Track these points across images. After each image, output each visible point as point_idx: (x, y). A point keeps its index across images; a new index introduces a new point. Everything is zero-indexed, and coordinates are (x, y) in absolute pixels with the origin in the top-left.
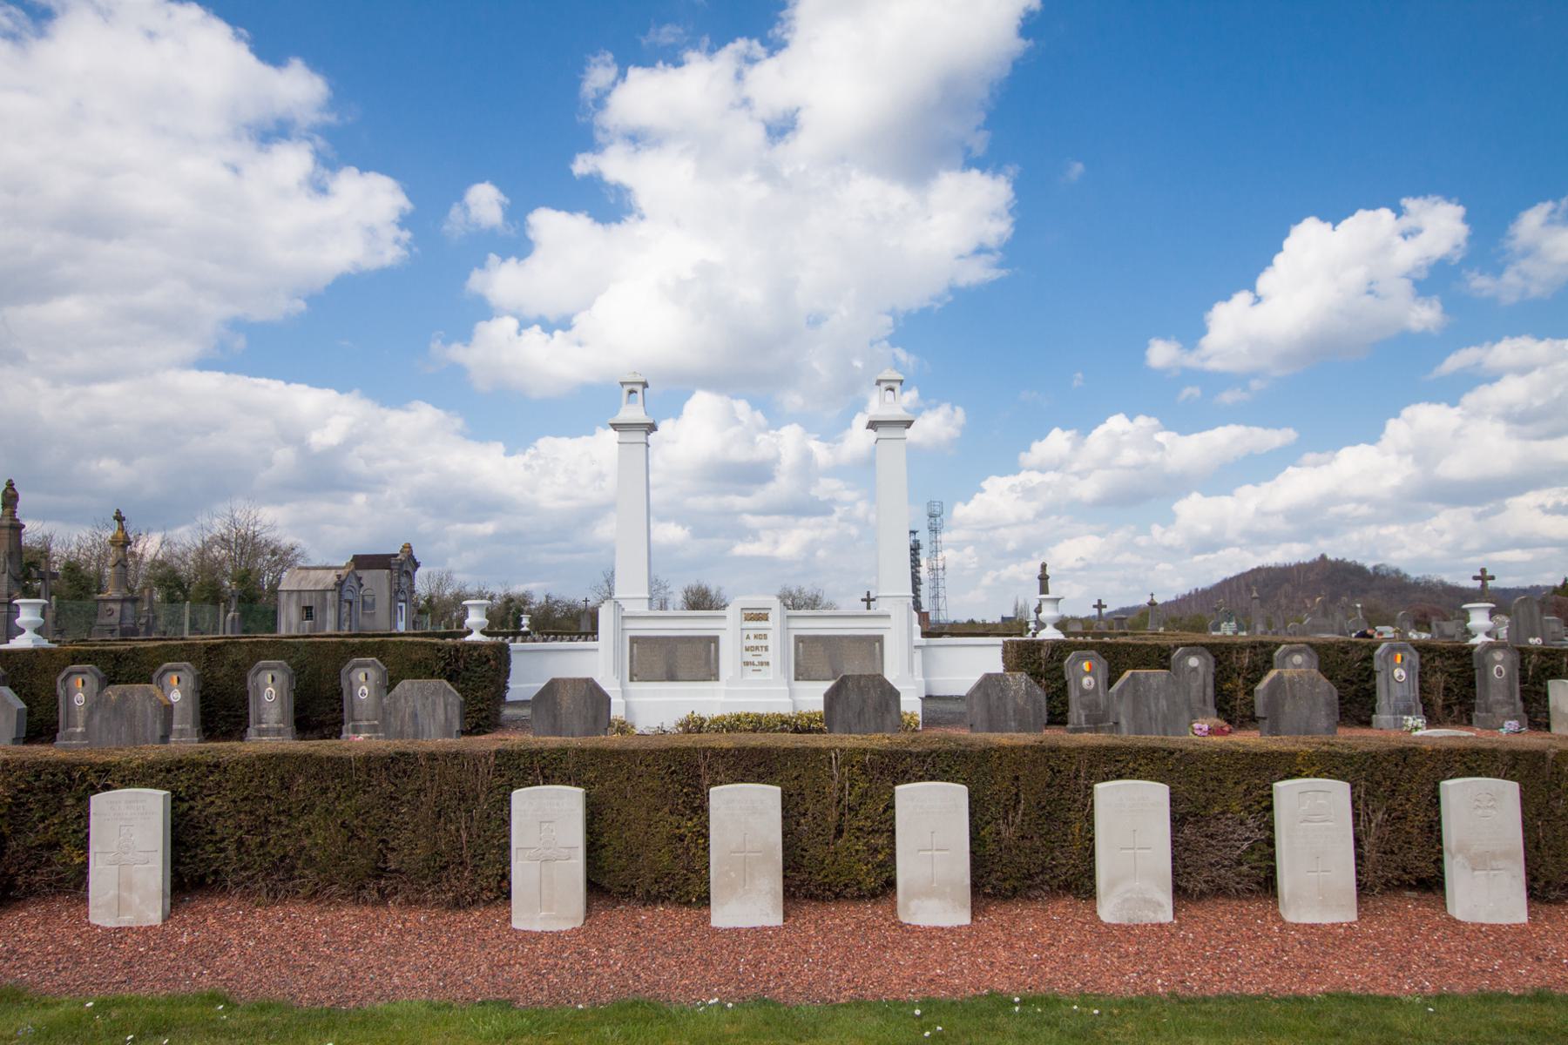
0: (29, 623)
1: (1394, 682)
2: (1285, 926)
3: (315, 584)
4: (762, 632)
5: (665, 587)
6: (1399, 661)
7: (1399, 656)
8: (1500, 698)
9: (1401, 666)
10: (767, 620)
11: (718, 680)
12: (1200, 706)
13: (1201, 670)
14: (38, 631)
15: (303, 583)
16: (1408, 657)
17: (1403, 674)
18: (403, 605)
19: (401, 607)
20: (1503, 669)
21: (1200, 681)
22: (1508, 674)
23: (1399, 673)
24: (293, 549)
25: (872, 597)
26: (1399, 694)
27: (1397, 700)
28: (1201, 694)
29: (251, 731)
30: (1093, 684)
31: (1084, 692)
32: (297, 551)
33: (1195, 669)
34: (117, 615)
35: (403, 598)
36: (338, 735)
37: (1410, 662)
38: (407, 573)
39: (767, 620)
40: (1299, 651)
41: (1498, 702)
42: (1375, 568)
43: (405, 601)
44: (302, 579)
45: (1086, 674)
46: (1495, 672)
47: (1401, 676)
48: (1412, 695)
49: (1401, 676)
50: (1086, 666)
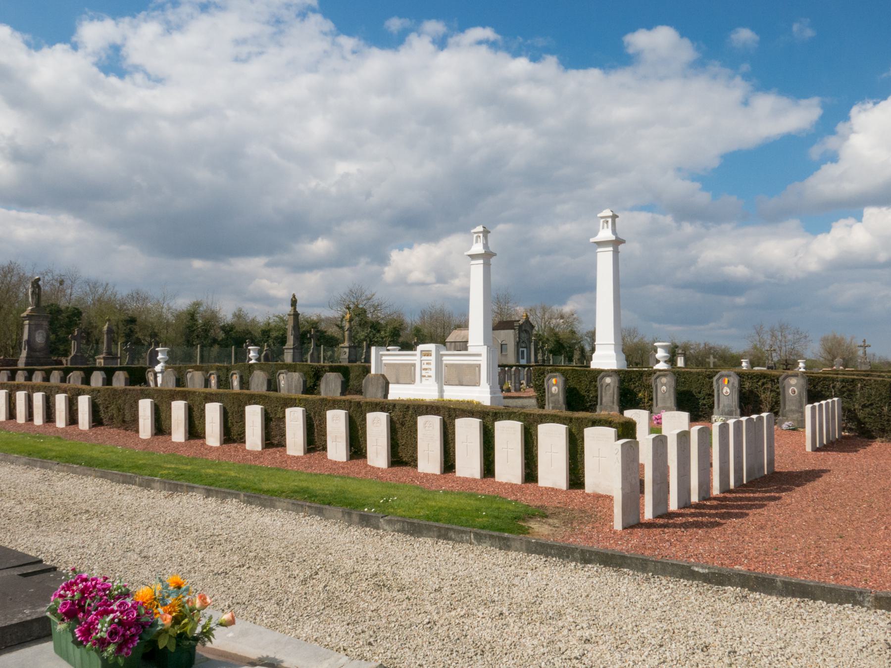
0: (253, 356)
1: (723, 396)
2: (367, 466)
3: (463, 338)
4: (429, 362)
5: (806, 337)
6: (726, 383)
7: (726, 380)
8: (794, 408)
9: (727, 386)
10: (431, 355)
11: (479, 386)
12: (611, 404)
13: (612, 385)
14: (804, 368)
15: (457, 338)
16: (732, 379)
17: (728, 391)
18: (525, 350)
19: (523, 352)
20: (796, 390)
21: (611, 391)
22: (800, 393)
23: (726, 390)
24: (573, 315)
25: (866, 344)
26: (726, 403)
27: (724, 406)
28: (612, 399)
29: (598, 407)
30: (557, 390)
31: (553, 395)
32: (575, 316)
33: (608, 385)
34: (347, 354)
35: (524, 345)
36: (594, 410)
37: (733, 383)
38: (526, 331)
39: (431, 355)
40: (665, 376)
41: (791, 411)
42: (238, 315)
43: (526, 347)
44: (457, 336)
45: (554, 385)
46: (790, 392)
47: (727, 392)
48: (734, 403)
49: (727, 392)
50: (554, 381)
